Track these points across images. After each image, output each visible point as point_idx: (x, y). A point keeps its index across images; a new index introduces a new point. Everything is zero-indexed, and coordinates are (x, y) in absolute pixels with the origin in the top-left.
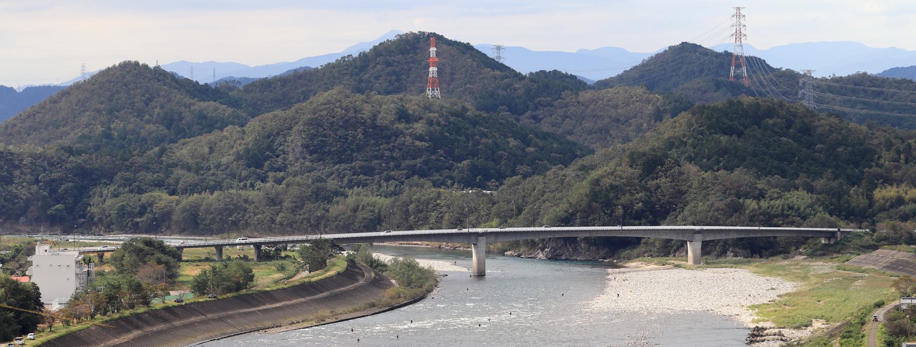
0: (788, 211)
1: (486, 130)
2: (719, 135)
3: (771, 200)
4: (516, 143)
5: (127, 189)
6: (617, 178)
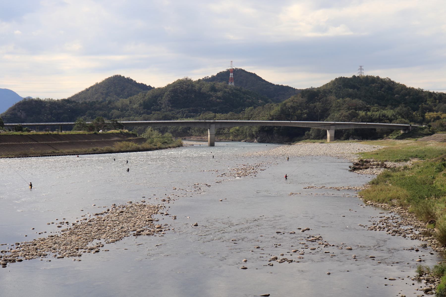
0: (382, 117)
1: (250, 96)
2: (348, 89)
3: (373, 112)
4: (262, 102)
5: (90, 117)
6: (295, 103)
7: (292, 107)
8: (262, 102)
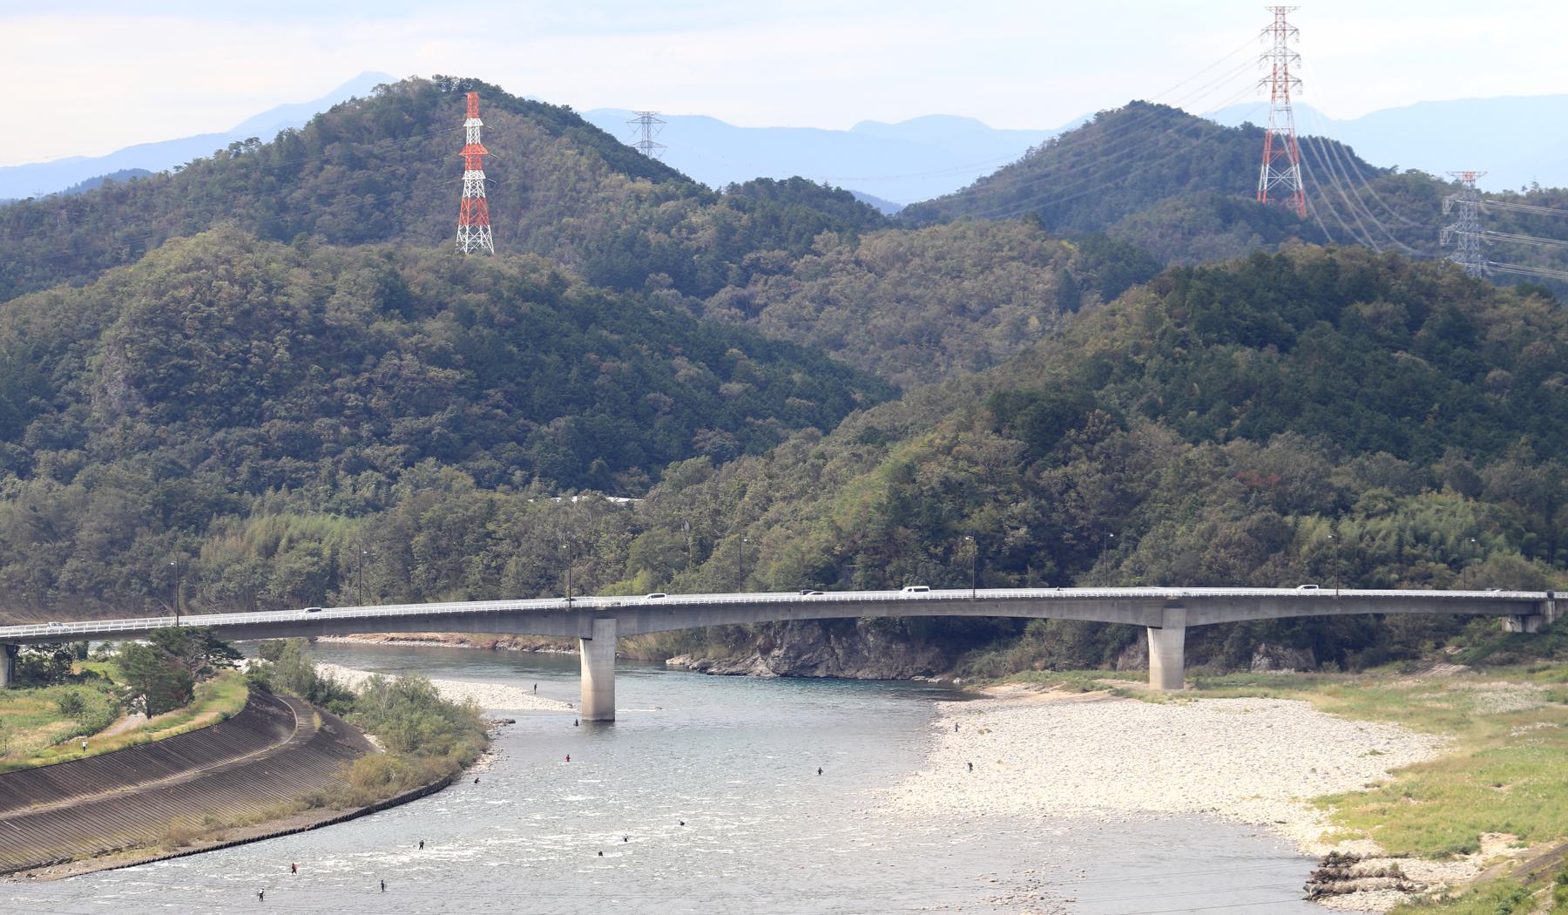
1: (616, 337)
2: (1230, 347)
3: (1368, 517)
4: (694, 371)
6: (961, 463)
7: (947, 484)
8: (694, 371)
